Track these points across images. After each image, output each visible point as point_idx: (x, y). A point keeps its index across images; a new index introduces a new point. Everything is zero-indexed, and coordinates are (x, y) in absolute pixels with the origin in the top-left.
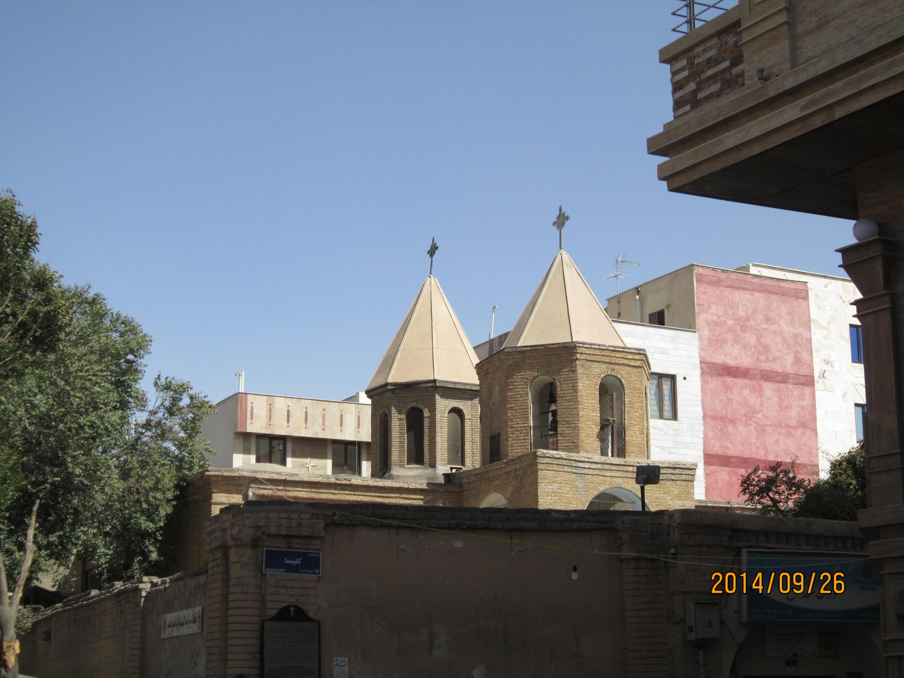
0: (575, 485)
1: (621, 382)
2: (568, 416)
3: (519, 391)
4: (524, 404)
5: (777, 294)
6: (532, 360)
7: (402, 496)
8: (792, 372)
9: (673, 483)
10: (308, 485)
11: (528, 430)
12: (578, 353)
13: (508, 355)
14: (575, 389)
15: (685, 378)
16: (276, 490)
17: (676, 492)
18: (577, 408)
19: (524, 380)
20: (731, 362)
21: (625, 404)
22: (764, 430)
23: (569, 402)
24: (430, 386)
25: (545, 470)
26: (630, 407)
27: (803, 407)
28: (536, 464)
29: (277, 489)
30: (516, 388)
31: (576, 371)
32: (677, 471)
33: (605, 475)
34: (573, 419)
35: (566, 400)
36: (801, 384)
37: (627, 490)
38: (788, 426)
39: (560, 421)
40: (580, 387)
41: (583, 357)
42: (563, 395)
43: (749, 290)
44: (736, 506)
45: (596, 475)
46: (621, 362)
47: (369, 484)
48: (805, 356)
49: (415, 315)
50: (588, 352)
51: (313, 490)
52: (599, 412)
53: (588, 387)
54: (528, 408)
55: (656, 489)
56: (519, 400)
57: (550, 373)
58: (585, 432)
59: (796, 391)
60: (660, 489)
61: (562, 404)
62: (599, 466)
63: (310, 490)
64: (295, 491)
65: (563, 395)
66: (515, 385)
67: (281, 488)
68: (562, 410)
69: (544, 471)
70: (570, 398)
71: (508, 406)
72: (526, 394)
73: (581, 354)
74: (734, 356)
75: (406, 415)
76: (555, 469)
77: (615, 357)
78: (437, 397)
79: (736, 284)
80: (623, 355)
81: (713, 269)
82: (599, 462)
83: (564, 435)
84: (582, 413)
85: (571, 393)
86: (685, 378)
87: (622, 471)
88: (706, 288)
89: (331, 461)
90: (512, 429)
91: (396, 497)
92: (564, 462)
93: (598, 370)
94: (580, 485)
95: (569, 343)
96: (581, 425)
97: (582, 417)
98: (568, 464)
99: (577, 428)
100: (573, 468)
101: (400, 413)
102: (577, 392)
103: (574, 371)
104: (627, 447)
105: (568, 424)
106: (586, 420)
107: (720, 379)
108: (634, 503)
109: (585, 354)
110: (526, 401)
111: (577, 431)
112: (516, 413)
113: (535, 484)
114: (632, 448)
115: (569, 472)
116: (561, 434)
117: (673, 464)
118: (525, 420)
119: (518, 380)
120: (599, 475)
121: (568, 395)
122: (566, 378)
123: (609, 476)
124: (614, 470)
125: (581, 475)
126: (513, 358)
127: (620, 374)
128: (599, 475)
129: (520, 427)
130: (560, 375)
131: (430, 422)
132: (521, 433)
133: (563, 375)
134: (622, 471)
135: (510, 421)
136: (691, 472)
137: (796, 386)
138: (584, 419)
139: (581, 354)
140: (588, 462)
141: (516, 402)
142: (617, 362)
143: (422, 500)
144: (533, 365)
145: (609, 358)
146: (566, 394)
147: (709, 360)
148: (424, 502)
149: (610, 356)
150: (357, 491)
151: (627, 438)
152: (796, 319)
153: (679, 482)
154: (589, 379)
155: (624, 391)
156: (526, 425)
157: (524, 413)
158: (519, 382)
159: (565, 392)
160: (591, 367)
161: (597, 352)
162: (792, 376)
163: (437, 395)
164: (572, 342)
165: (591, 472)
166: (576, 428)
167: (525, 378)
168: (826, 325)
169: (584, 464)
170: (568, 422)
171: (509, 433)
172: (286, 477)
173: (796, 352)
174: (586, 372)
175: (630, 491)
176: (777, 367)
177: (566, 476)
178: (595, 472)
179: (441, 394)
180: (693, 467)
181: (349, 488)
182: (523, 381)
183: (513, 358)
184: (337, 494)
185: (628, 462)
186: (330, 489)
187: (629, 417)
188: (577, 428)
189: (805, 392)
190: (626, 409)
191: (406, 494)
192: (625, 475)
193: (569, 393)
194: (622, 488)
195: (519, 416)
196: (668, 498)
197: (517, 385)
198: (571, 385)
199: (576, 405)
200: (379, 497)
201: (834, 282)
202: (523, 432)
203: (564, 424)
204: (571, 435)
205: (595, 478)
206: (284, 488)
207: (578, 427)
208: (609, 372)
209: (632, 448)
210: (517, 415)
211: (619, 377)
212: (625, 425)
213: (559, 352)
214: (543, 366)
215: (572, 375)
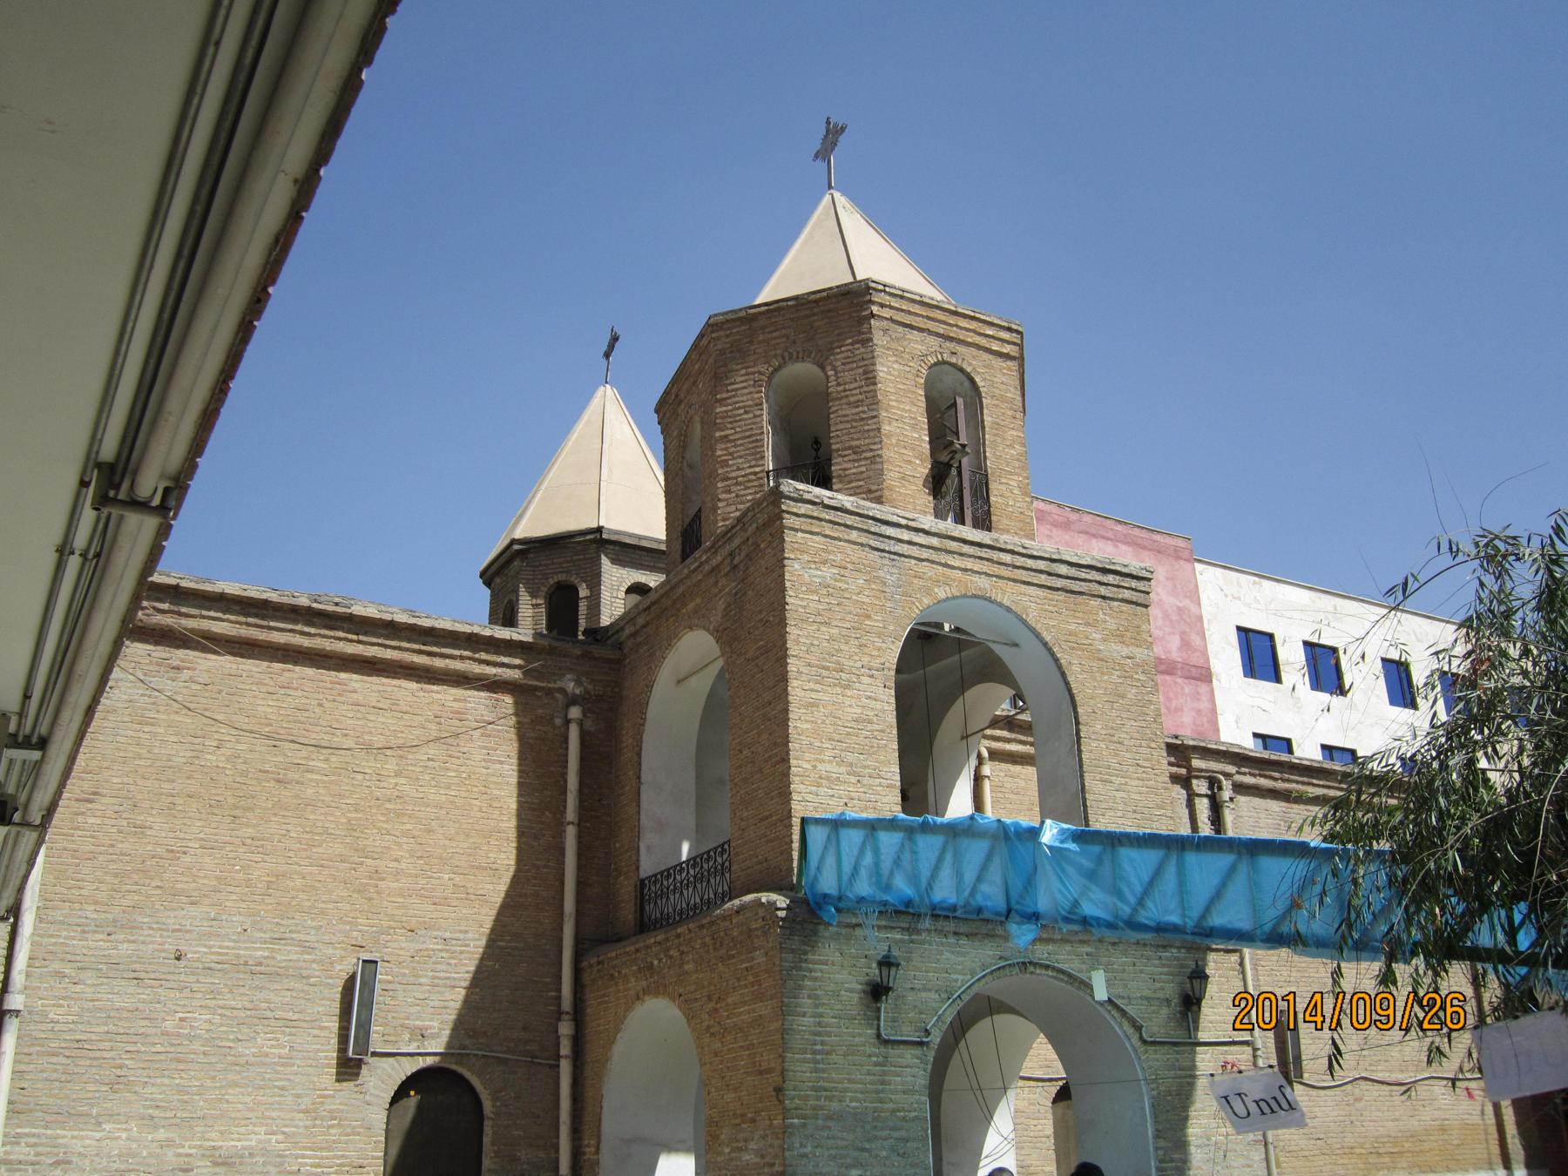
0: (878, 577)
1: (972, 381)
2: (855, 436)
3: (743, 401)
4: (754, 426)
5: (1150, 550)
6: (772, 332)
7: (477, 656)
8: (1180, 660)
9: (1104, 604)
10: (237, 608)
11: (761, 478)
12: (873, 303)
13: (717, 331)
14: (870, 378)
16: (151, 611)
17: (1112, 624)
18: (875, 417)
19: (752, 377)
21: (983, 427)
23: (857, 407)
24: (590, 540)
25: (803, 531)
26: (995, 435)
27: (1199, 712)
28: (779, 516)
29: (154, 608)
30: (734, 396)
31: (871, 340)
32: (1110, 578)
33: (949, 562)
34: (867, 441)
35: (849, 404)
36: (1194, 679)
37: (1000, 605)
39: (838, 450)
40: (881, 374)
41: (886, 313)
42: (843, 394)
43: (1111, 540)
44: (1191, 743)
45: (927, 560)
46: (969, 340)
47: (395, 619)
48: (1195, 640)
49: (570, 443)
50: (897, 305)
51: (250, 620)
52: (927, 433)
53: (899, 376)
54: (763, 446)
55: (1067, 612)
56: (740, 420)
57: (810, 353)
58: (898, 469)
59: (1188, 688)
60: (1077, 614)
61: (840, 413)
62: (935, 541)
63: (242, 619)
64: (203, 617)
65: (843, 394)
66: (732, 390)
67: (165, 606)
68: (841, 426)
69: (800, 534)
70: (860, 397)
71: (718, 434)
72: (756, 405)
73: (882, 306)
75: (545, 598)
76: (827, 533)
77: (957, 326)
78: (605, 561)
79: (1092, 530)
80: (973, 325)
81: (1059, 505)
82: (933, 530)
83: (847, 479)
84: (887, 428)
85: (860, 387)
87: (988, 560)
88: (1051, 531)
90: (726, 483)
91: (462, 658)
92: (850, 520)
93: (920, 347)
94: (891, 579)
95: (851, 283)
97: (889, 436)
98: (860, 526)
99: (878, 460)
100: (870, 536)
101: (533, 595)
102: (875, 384)
103: (867, 341)
104: (994, 518)
105: (855, 453)
108: (1016, 645)
109: (891, 307)
110: (758, 419)
111: (879, 466)
112: (735, 446)
113: (778, 565)
114: (1005, 521)
115: (862, 545)
116: (840, 476)
117: (1101, 562)
118: (756, 460)
119: (739, 379)
120: (933, 562)
121: (854, 392)
122: (849, 357)
123: (961, 569)
124: (970, 556)
125: (892, 557)
126: (728, 336)
127: (970, 364)
128: (933, 562)
129: (743, 476)
130: (834, 354)
131: (589, 608)
132: (746, 488)
133: (842, 352)
134: (988, 560)
135: (722, 467)
136: (1141, 585)
137: (1186, 681)
138: (894, 441)
139: (882, 306)
140: (908, 528)
141: (735, 425)
142: (961, 337)
143: (518, 667)
144: (773, 342)
145: (945, 327)
146: (850, 390)
148: (524, 673)
149: (945, 323)
150: (365, 634)
151: (992, 499)
152: (1178, 586)
153: (1116, 603)
154: (900, 360)
155: (981, 403)
156: (757, 469)
157: (754, 445)
158: (742, 382)
159: (847, 387)
160: (904, 338)
161: (916, 309)
162: (1179, 665)
163: (603, 557)
164: (856, 281)
165: (915, 551)
166: (875, 459)
167: (754, 373)
169: (898, 530)
170: (856, 450)
171: (719, 491)
172: (179, 581)
173: (1183, 633)
174: (893, 345)
175: (1009, 609)
177: (856, 554)
178: (925, 554)
179: (613, 556)
180: (1147, 575)
181: (346, 626)
182: (750, 380)
183: (728, 336)
184: (315, 635)
185: (1002, 541)
186: (295, 622)
187: (994, 454)
188: (878, 460)
189: (1201, 691)
190: (987, 436)
191: (487, 652)
192: (996, 570)
193: (855, 388)
194: (989, 600)
195: (743, 453)
196: (1094, 635)
197: (737, 390)
198: (861, 370)
199: (873, 410)
200: (420, 652)
201: (1210, 568)
202: (751, 484)
203: (845, 456)
204: (864, 475)
205: (924, 568)
206: (172, 607)
207: (880, 456)
208: (945, 355)
210: (738, 452)
211: (969, 370)
212: (986, 471)
213: (831, 306)
214: (794, 342)
215: (863, 350)
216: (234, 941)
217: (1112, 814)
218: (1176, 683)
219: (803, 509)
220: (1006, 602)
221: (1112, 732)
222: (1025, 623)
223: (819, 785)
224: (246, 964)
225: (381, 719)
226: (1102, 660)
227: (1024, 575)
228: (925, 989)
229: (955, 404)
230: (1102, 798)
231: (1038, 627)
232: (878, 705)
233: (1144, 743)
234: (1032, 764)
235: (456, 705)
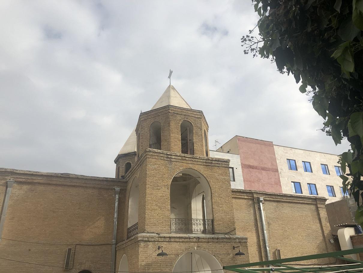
15: (236, 169)
17: (220, 172)
20: (251, 164)
22: (264, 185)
27: (276, 178)
32: (220, 163)
36: (274, 171)
37: (195, 170)
38: (271, 184)
69: (150, 159)
73: (172, 110)
74: (252, 162)
76: (156, 158)
86: (236, 169)
89: (259, 261)
96: (171, 140)
106: (174, 138)
107: (248, 169)
108: (200, 178)
114: (197, 152)
127: (191, 120)
147: (244, 163)
168: (279, 159)
175: (196, 170)
176: (266, 166)
177: (163, 162)
209: (197, 152)
216: (42, 246)
217: (219, 213)
218: (270, 173)
219: (151, 153)
220: (196, 169)
221: (219, 195)
222: (200, 173)
223: (152, 211)
224: (44, 251)
225: (76, 198)
226: (218, 180)
227: (200, 163)
228: (172, 254)
229: (187, 129)
230: (217, 210)
231: (203, 174)
232: (166, 193)
233: (227, 197)
234: (234, 191)
235: (92, 194)
